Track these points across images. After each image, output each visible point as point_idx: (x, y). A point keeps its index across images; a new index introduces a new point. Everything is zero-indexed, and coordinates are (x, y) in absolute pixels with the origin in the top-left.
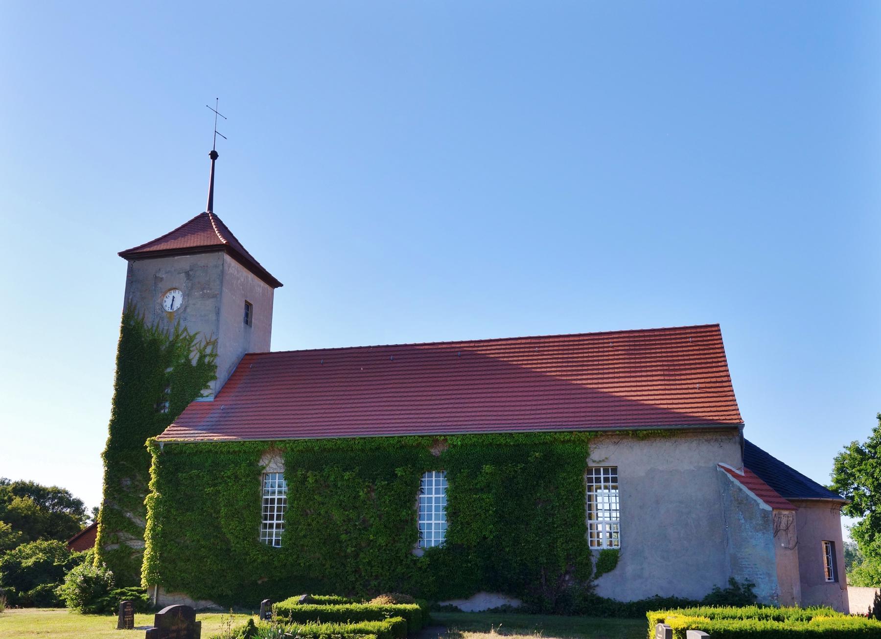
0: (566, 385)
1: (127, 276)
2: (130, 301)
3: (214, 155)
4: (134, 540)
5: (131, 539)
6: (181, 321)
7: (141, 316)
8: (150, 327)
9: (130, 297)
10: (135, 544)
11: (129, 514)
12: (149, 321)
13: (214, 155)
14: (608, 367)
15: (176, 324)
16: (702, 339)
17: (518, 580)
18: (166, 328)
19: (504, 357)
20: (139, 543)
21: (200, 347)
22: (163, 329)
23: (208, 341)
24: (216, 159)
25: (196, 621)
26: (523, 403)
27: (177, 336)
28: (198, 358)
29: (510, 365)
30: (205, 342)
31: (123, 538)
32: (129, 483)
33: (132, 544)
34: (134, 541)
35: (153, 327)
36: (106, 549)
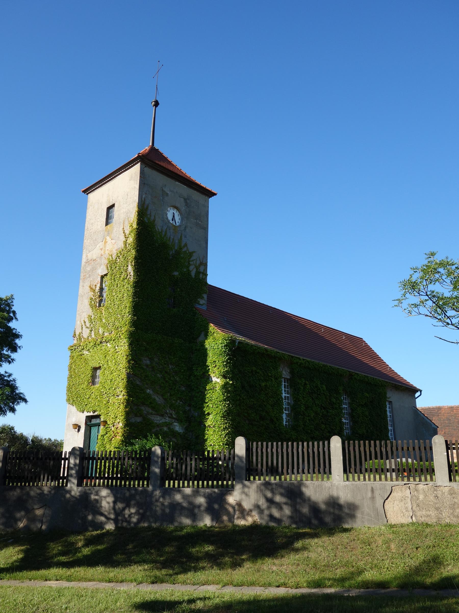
0: (366, 364)
1: (140, 177)
2: (143, 199)
3: (157, 104)
4: (154, 414)
5: (152, 414)
6: (183, 238)
7: (152, 218)
8: (160, 231)
9: (144, 196)
10: (155, 419)
11: (148, 390)
12: (159, 226)
13: (157, 104)
14: (300, 332)
15: (179, 237)
16: (327, 332)
17: (186, 402)
18: (172, 237)
19: (315, 330)
20: (158, 418)
21: (196, 263)
22: (170, 237)
23: (201, 262)
24: (157, 107)
25: (82, 447)
26: (320, 355)
27: (181, 249)
28: (195, 272)
29: (323, 338)
30: (199, 262)
31: (145, 412)
32: (148, 362)
33: (153, 418)
34: (155, 416)
35: (162, 230)
36: (131, 421)
